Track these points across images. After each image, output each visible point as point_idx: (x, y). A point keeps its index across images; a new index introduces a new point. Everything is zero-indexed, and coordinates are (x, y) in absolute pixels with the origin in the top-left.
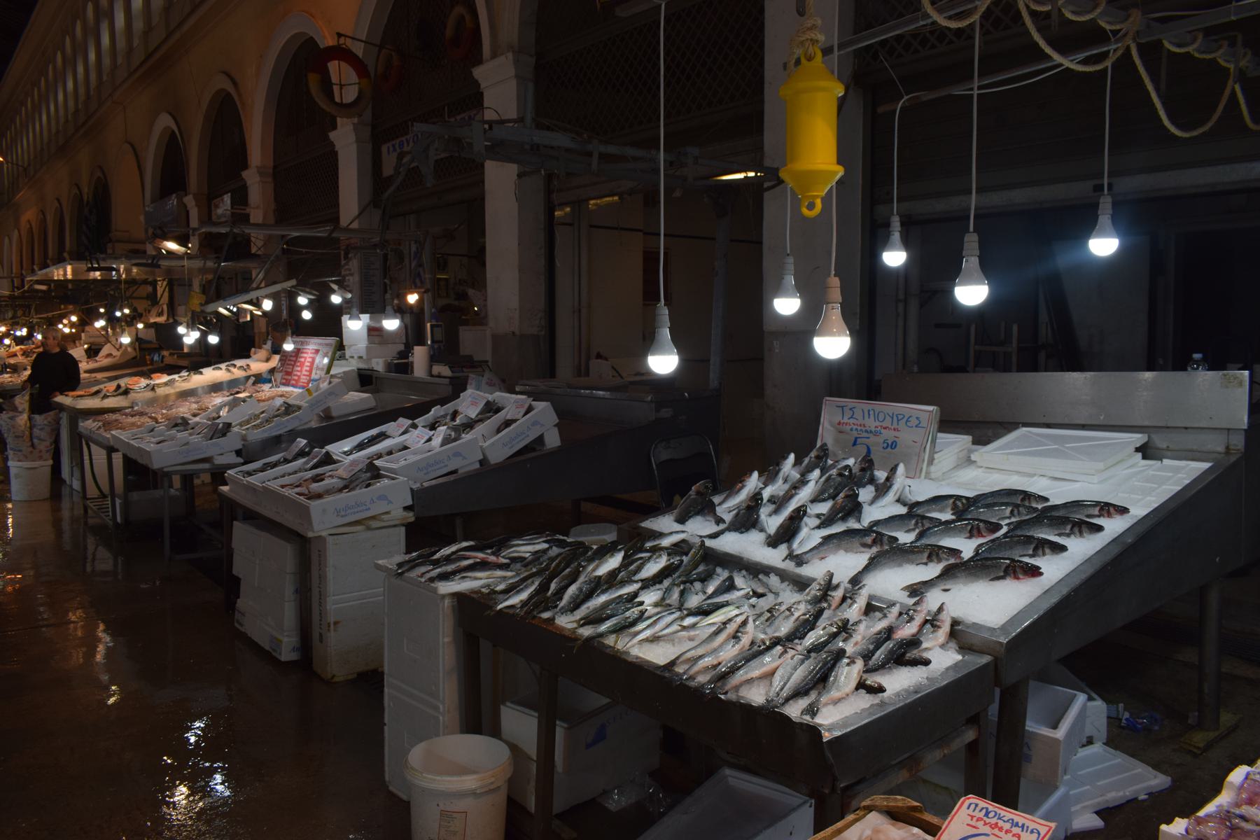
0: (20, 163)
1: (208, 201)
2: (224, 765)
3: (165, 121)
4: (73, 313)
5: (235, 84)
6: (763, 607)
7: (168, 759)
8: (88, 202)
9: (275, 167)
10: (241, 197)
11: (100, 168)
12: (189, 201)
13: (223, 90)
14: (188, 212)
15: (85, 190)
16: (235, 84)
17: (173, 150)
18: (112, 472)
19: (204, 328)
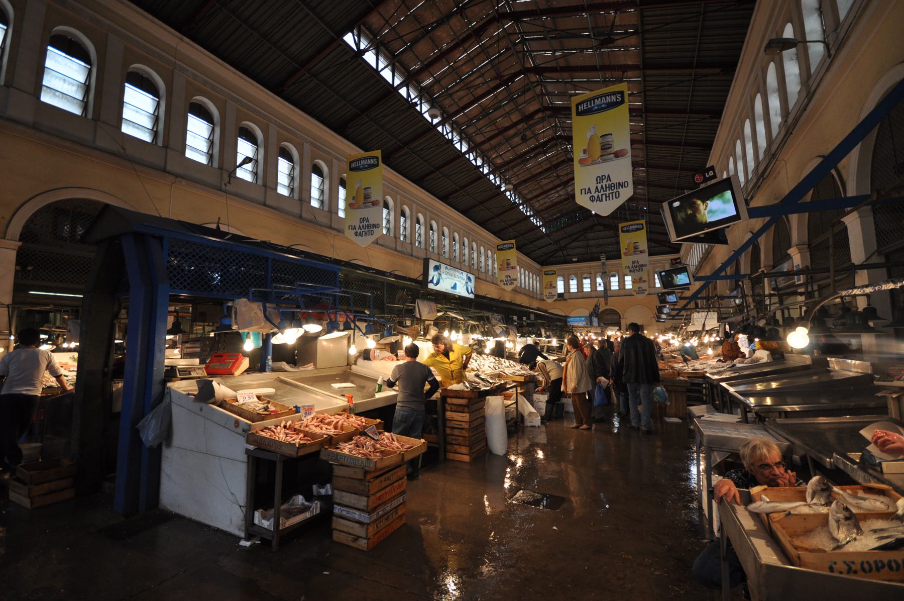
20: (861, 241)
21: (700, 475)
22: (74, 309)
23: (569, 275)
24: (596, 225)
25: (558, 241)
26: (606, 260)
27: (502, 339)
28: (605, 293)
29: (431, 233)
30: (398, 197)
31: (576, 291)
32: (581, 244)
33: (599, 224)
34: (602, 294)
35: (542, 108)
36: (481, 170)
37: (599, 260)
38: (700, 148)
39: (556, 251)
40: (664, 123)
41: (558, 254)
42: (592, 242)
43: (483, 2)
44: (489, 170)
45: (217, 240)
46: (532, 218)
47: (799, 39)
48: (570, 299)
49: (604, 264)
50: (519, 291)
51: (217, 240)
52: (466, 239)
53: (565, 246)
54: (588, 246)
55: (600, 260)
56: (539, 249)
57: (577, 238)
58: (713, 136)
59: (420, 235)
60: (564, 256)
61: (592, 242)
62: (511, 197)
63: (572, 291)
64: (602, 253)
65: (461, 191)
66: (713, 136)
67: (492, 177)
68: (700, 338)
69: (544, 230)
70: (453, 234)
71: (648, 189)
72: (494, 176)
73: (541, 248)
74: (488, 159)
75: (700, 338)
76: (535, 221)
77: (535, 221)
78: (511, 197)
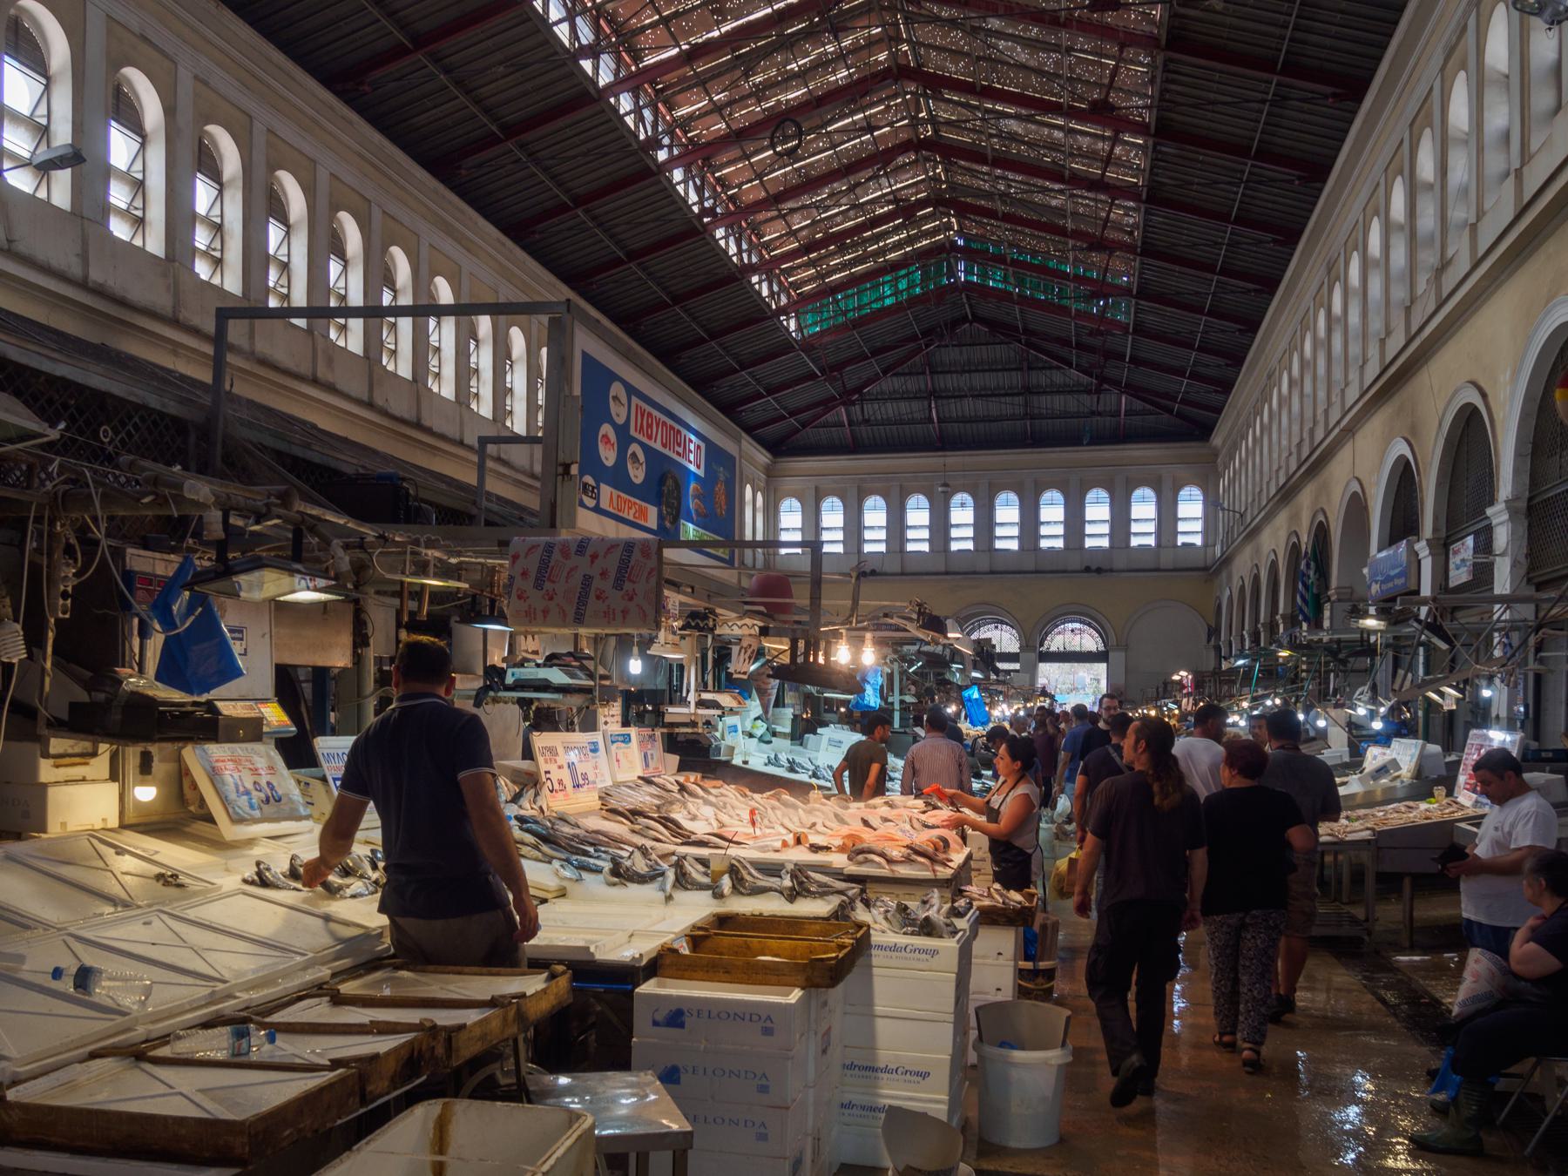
0: (1237, 509)
1: (1443, 547)
2: (812, 22)
3: (1400, 448)
4: (1276, 695)
5: (1484, 395)
6: (589, 790)
7: (1149, 710)
8: (1306, 553)
9: (1530, 499)
10: (1485, 544)
11: (1323, 510)
12: (1422, 548)
13: (1468, 405)
14: (1419, 562)
15: (1304, 538)
16: (1484, 395)
17: (1404, 479)
18: (54, 997)
19: (1133, 1014)
20: (51, 1169)
21: (1032, 298)
24: (964, 319)
25: (840, 366)
27: (1471, 757)
29: (472, 347)
30: (377, 214)
32: (912, 384)
33: (977, 318)
35: (895, 70)
36: (587, 65)
38: (1329, 90)
39: (828, 404)
40: (1210, 115)
41: (829, 417)
42: (949, 382)
44: (616, 73)
46: (755, 279)
47: (1526, 16)
50: (451, 430)
52: (398, 253)
53: (859, 390)
56: (771, 391)
57: (901, 362)
59: (218, 229)
61: (949, 382)
62: (640, 119)
65: (510, 145)
67: (678, 175)
69: (792, 325)
70: (332, 217)
71: (1147, 212)
72: (636, 98)
73: (753, 364)
74: (617, 30)
76: (733, 249)
77: (733, 249)
78: (640, 119)
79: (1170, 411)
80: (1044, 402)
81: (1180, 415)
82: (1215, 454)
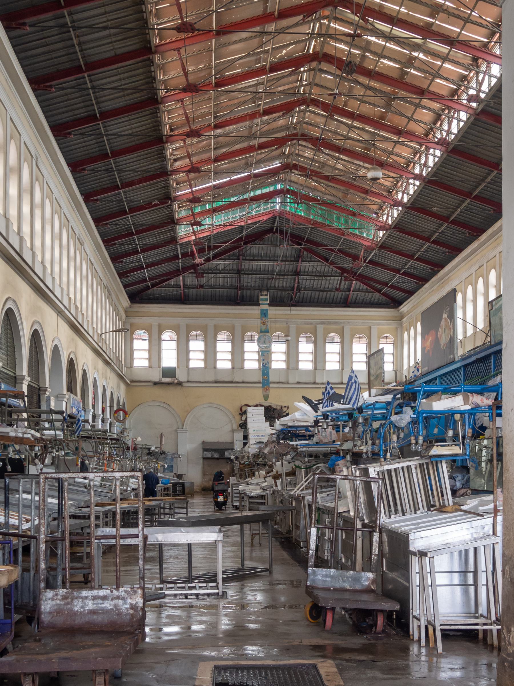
22: (478, 109)
23: (189, 329)
26: (270, 305)
28: (264, 374)
31: (201, 365)
34: (258, 377)
37: (256, 303)
41: (172, 282)
43: (121, 1)
45: (420, 74)
48: (188, 382)
49: (264, 314)
51: (420, 74)
54: (297, 273)
55: (259, 305)
58: (440, 168)
60: (185, 286)
63: (220, 365)
64: (261, 290)
66: (440, 168)
68: (205, 490)
75: (205, 490)
79: (379, 291)
80: (306, 282)
81: (384, 294)
82: (401, 317)
